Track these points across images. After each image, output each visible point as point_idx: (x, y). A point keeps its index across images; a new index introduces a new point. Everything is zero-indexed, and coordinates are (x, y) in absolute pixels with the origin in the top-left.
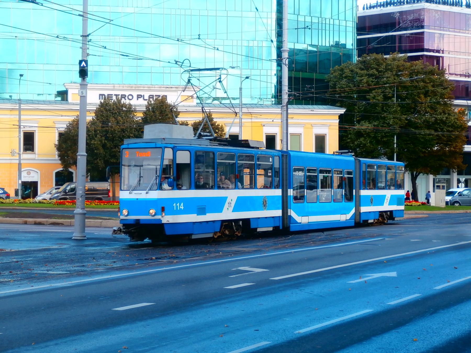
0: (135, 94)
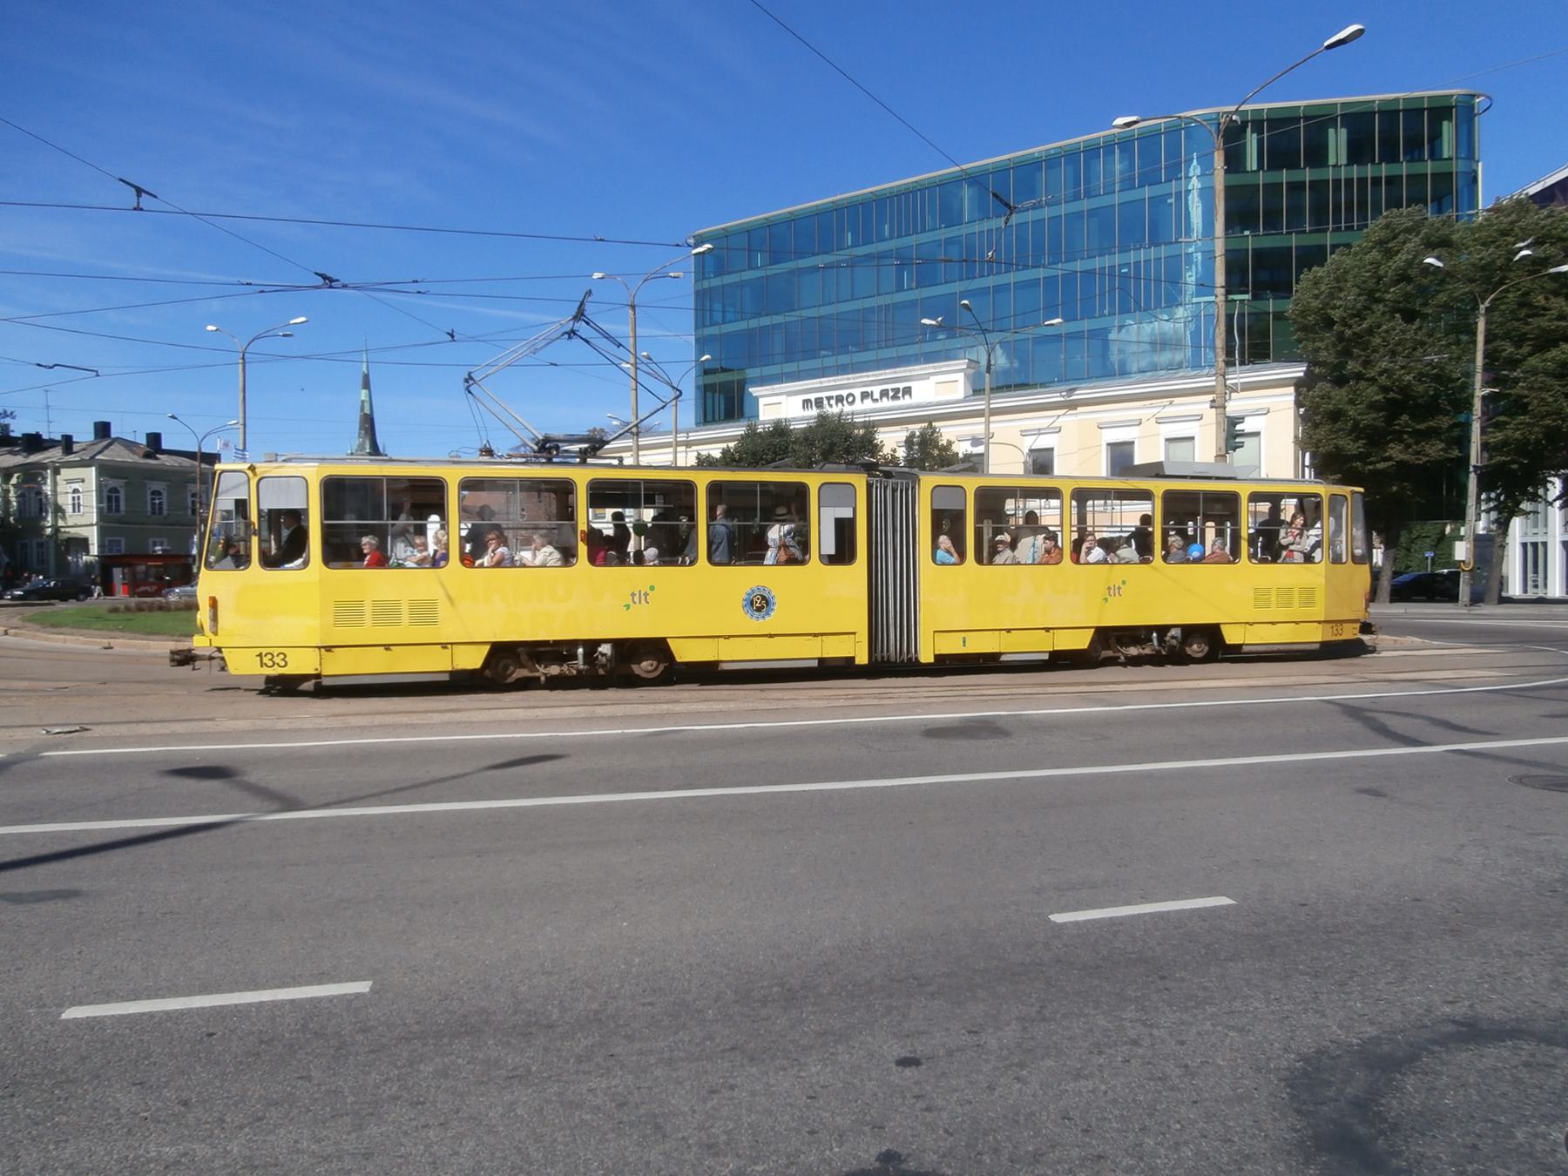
0: (857, 392)
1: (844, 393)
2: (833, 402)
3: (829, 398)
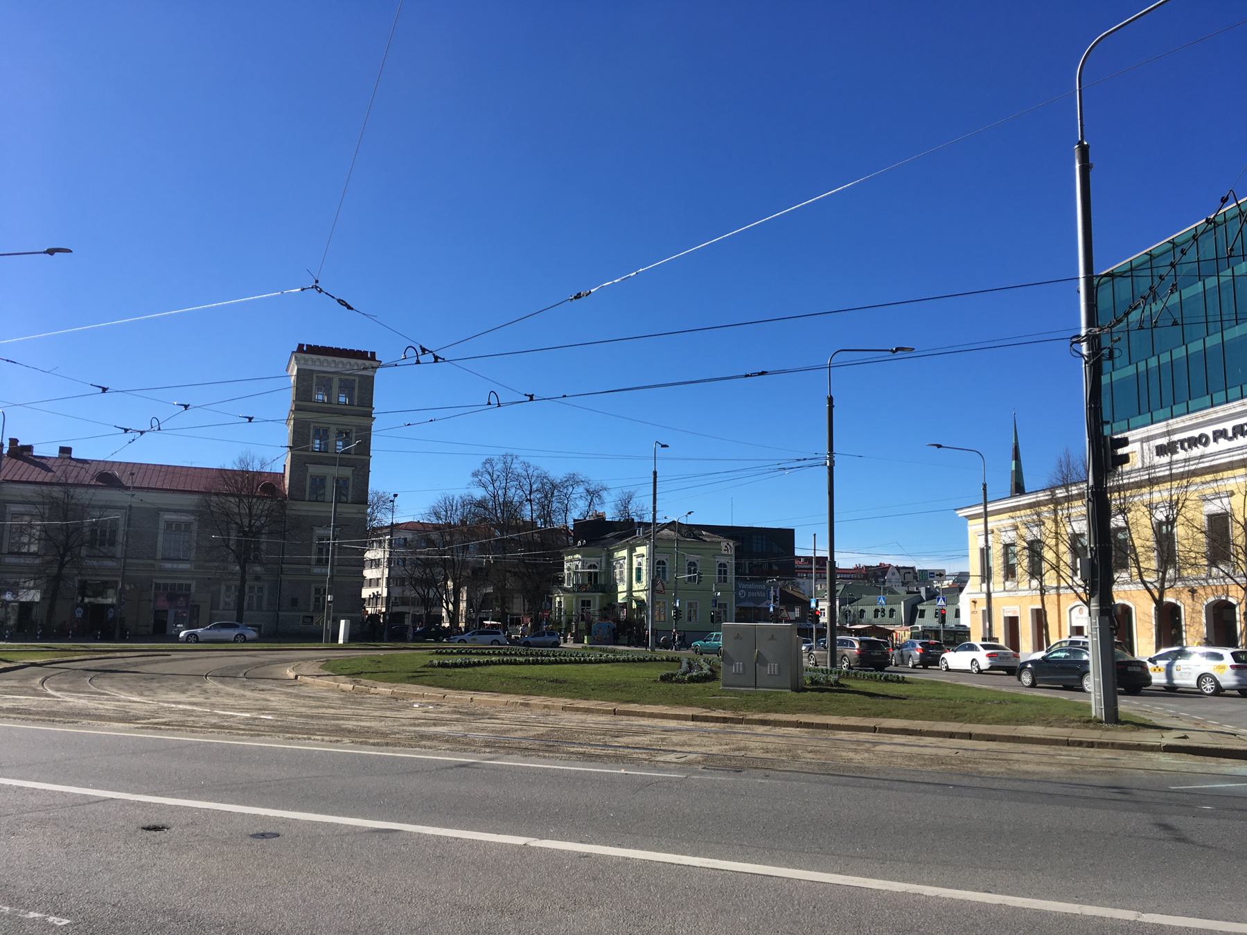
1: (1195, 433)
2: (1186, 445)
3: (1182, 442)
